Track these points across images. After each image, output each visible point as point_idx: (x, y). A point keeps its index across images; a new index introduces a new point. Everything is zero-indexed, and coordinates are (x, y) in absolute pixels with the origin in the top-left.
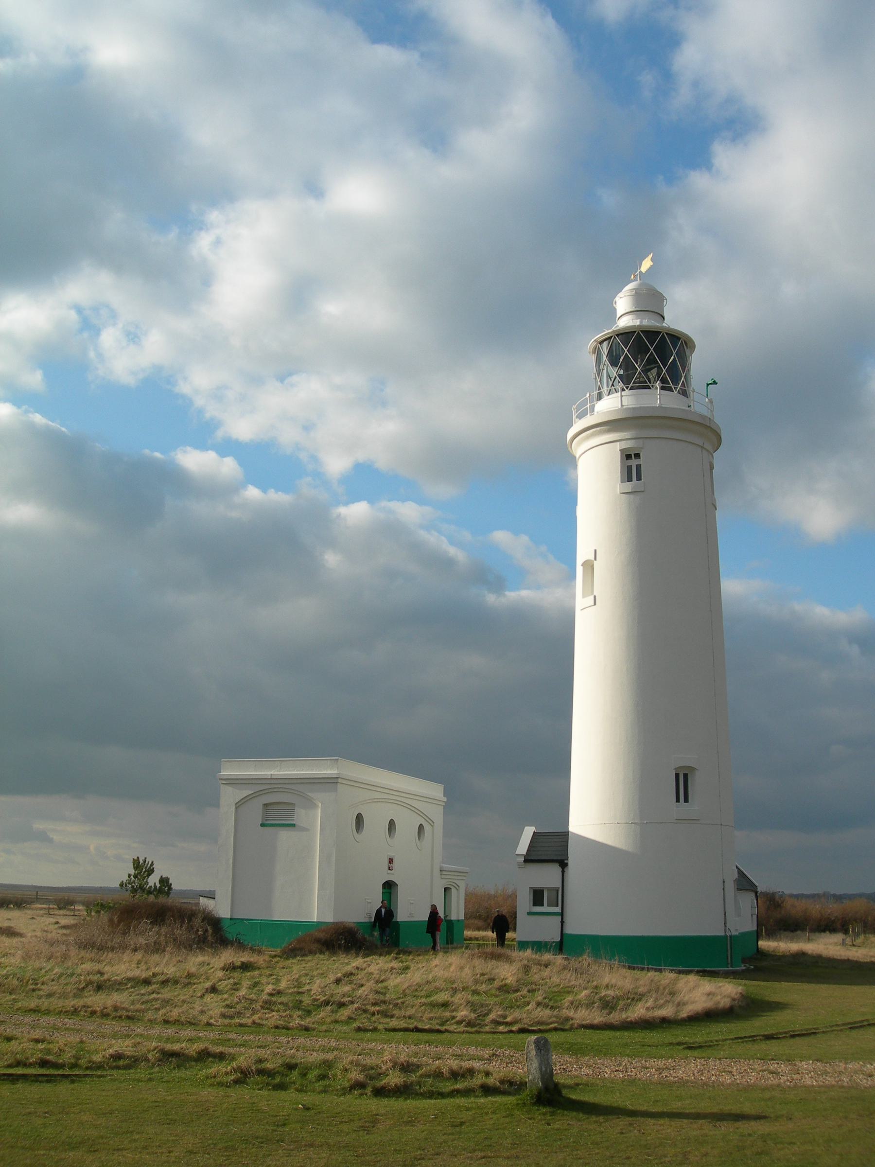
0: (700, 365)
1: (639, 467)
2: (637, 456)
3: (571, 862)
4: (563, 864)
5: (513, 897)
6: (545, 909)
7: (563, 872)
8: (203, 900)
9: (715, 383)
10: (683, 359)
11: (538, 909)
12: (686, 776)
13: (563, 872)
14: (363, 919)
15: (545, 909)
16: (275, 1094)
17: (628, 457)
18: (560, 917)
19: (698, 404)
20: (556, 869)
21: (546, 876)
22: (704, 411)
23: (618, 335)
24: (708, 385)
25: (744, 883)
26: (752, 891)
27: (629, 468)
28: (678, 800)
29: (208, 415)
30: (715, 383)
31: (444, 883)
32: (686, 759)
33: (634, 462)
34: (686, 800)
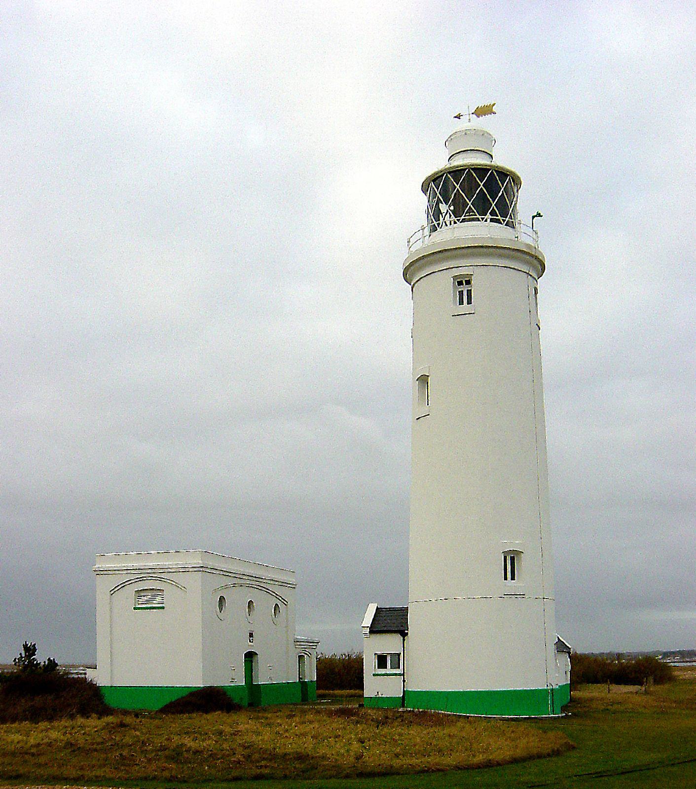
0: (525, 203)
1: (469, 292)
2: (468, 282)
3: (410, 632)
4: (404, 634)
5: (359, 661)
6: (389, 670)
7: (404, 640)
8: (88, 671)
9: (539, 215)
10: (511, 194)
11: (383, 671)
12: (513, 559)
13: (404, 640)
14: (425, 199)
15: (389, 670)
16: (491, 133)
17: (460, 283)
18: (402, 677)
19: (523, 236)
20: (398, 638)
21: (389, 644)
22: (529, 241)
23: (450, 173)
24: (533, 217)
25: (561, 647)
26: (567, 652)
27: (461, 293)
28: (506, 579)
29: (262, 699)
30: (539, 215)
31: (299, 651)
32: (515, 544)
33: (464, 288)
34: (513, 578)
